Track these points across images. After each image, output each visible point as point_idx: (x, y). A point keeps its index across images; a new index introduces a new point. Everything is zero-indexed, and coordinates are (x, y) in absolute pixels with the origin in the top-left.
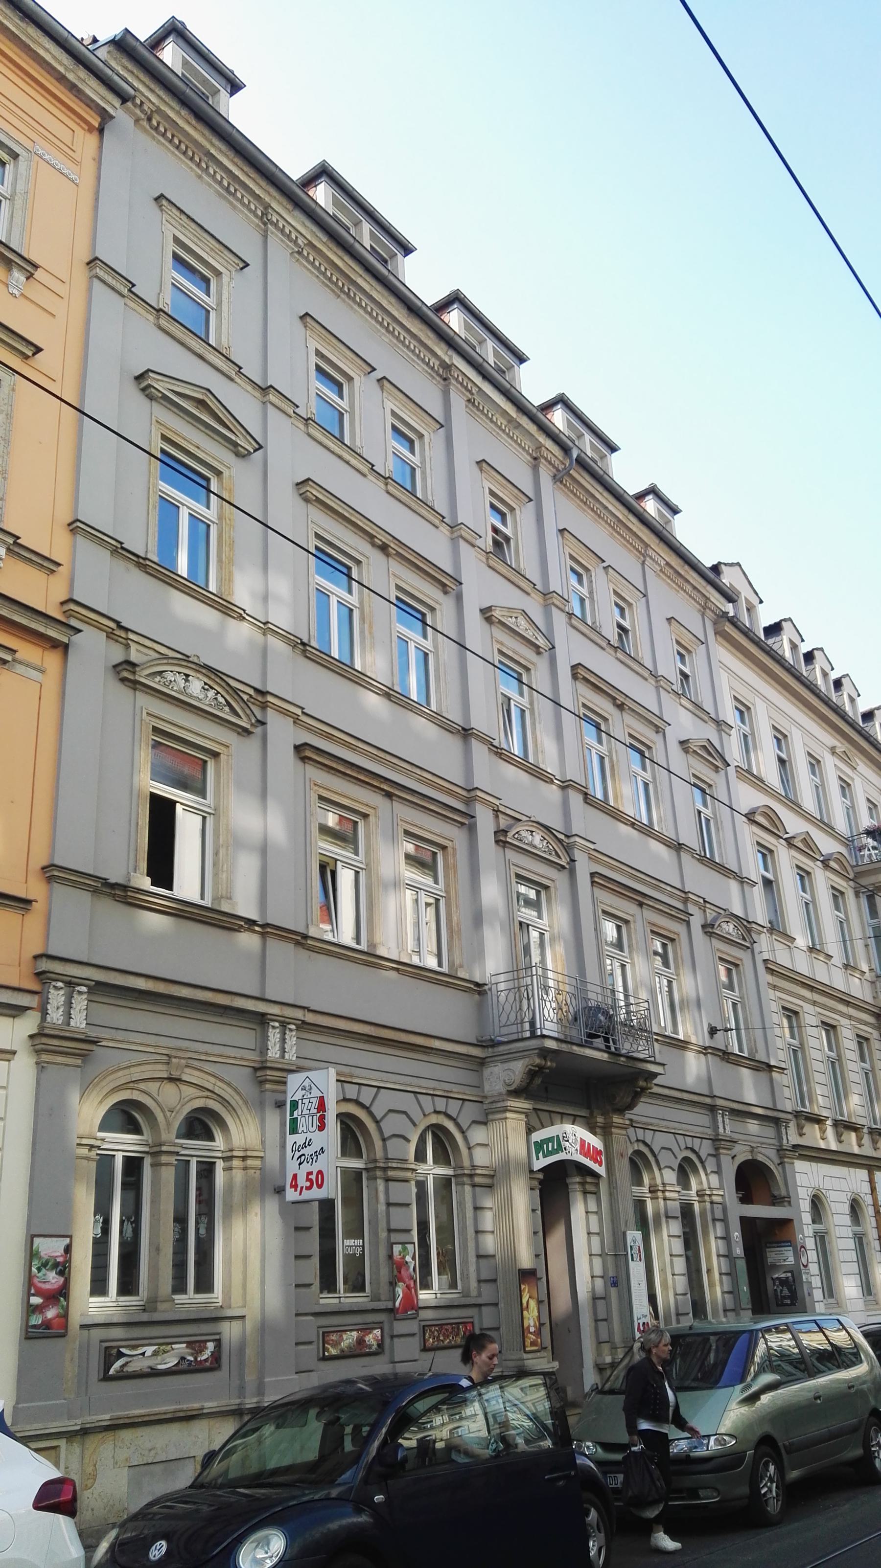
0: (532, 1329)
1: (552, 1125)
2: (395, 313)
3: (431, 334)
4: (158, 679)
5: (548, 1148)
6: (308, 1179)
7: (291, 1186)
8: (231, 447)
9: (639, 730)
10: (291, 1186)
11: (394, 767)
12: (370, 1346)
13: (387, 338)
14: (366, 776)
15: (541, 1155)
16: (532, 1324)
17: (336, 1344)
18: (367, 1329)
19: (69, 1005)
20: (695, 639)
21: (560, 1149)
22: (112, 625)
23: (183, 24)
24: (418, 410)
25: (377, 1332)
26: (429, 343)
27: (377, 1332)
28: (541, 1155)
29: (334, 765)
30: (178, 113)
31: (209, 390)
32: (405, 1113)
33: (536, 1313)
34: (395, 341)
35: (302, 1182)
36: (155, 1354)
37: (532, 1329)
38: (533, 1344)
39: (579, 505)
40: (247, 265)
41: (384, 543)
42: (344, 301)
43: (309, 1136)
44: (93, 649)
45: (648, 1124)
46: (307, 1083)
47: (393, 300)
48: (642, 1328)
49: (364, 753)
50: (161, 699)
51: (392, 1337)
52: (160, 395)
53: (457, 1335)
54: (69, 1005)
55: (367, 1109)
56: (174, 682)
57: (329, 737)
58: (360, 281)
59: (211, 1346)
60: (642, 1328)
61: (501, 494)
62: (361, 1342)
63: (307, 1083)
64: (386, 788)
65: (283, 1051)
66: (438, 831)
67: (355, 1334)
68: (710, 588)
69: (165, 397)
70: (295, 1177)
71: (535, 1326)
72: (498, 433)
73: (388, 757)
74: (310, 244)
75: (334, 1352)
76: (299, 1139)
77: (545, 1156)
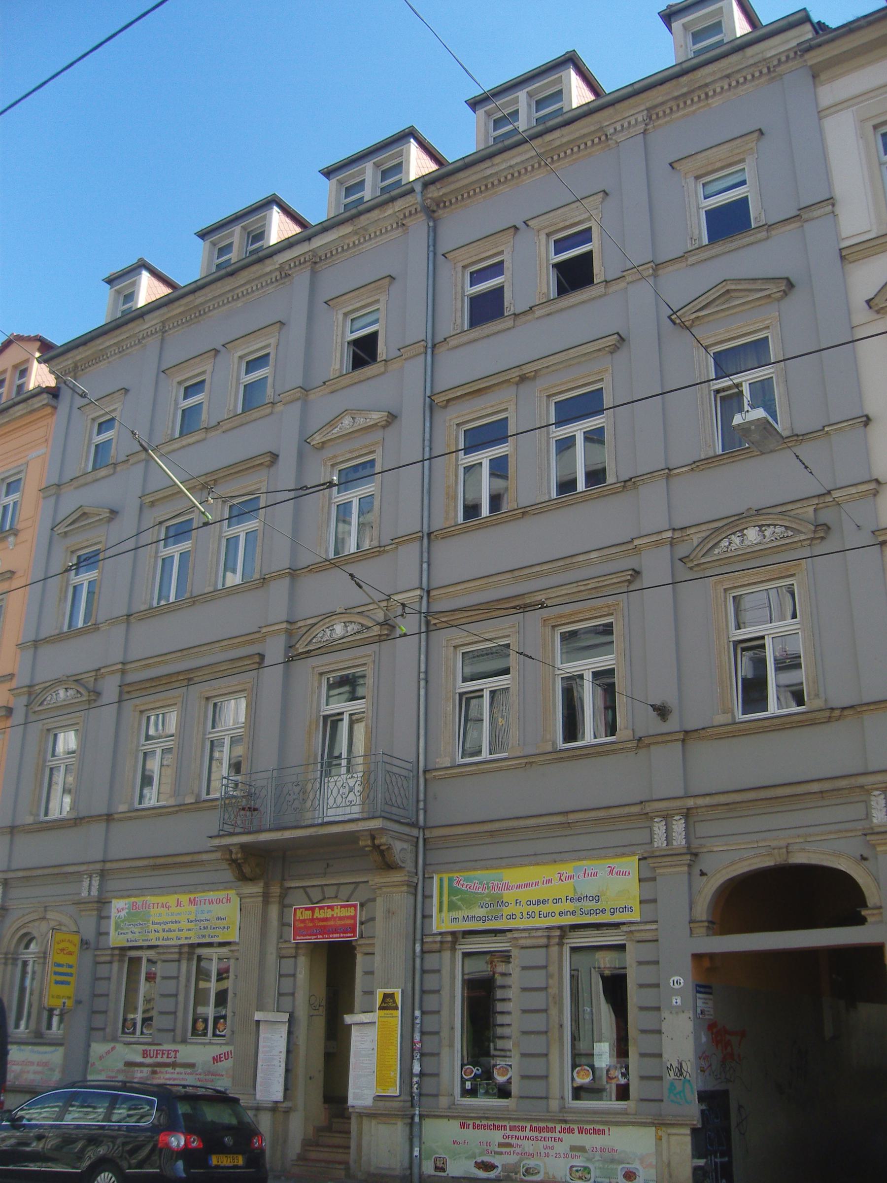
23: (669, 7)
29: (143, 686)
40: (671, 164)
41: (519, 376)
57: (147, 666)
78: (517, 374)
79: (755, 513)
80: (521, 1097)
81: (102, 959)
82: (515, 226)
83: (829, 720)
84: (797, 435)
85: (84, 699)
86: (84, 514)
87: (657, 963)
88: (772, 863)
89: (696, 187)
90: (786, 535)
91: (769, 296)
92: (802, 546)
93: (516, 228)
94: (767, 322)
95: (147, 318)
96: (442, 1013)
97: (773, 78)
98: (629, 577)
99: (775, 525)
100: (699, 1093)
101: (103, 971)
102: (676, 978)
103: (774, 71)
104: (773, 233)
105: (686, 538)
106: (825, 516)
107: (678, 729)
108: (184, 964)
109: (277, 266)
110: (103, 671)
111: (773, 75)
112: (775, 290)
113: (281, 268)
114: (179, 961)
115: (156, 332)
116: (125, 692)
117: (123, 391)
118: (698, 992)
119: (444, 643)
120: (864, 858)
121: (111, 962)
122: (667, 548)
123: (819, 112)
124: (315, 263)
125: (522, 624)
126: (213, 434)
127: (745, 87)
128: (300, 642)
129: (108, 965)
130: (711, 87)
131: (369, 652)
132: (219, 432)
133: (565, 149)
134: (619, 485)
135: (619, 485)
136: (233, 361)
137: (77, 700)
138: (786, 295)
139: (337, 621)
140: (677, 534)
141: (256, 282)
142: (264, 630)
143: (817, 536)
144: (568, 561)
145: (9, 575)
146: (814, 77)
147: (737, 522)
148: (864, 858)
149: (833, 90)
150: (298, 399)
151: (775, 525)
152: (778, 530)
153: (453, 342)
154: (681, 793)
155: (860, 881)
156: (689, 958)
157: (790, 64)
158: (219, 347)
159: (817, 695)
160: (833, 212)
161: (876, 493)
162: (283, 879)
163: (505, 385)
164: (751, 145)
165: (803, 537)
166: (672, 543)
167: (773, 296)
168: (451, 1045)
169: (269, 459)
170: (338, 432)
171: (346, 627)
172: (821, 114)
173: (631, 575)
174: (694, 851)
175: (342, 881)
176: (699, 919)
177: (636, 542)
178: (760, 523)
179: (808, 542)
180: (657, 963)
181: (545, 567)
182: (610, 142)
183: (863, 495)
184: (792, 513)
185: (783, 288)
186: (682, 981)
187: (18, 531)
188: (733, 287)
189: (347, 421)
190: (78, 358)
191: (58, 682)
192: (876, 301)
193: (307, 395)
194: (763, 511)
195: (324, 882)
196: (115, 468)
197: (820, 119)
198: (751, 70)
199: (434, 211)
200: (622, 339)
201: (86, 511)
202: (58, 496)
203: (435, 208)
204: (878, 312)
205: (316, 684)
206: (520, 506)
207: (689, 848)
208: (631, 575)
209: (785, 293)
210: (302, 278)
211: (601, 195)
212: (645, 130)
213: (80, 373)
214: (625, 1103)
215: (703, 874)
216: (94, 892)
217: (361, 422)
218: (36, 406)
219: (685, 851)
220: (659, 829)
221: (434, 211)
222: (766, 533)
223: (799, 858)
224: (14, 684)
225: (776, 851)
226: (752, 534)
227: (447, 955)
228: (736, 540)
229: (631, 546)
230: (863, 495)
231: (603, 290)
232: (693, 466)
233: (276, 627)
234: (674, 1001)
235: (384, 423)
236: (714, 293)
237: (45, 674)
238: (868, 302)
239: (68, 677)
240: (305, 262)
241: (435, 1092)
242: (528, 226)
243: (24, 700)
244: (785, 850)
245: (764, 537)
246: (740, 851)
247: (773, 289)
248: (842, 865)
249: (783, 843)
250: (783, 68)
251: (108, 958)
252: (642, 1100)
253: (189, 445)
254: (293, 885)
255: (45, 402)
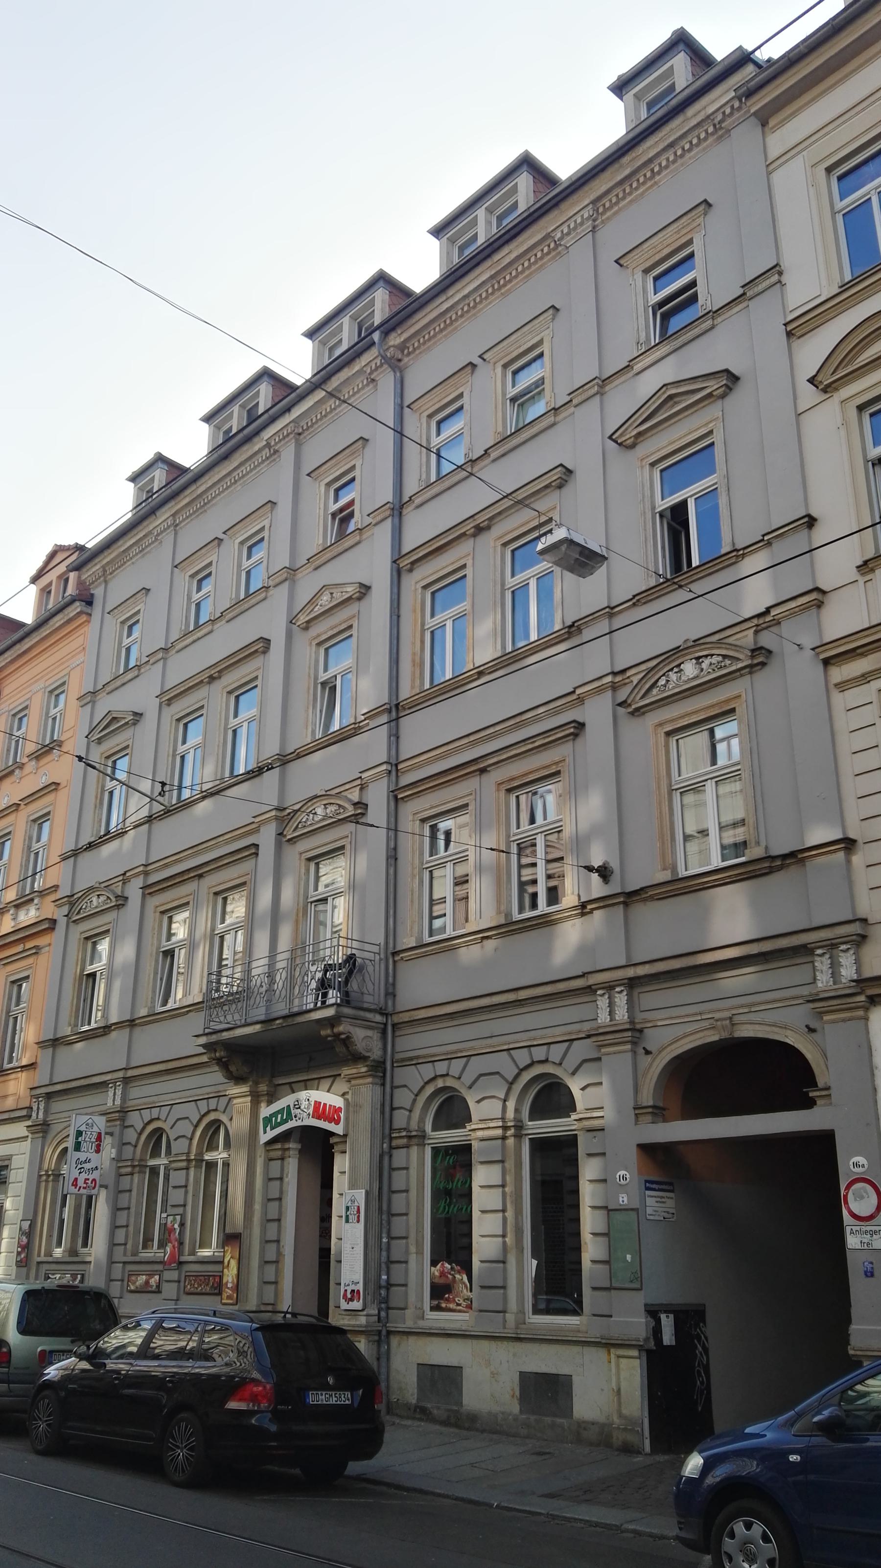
0: (230, 1285)
1: (317, 1089)
2: (224, 473)
3: (245, 448)
4: (655, 691)
5: (276, 1119)
6: (85, 1183)
7: (73, 1185)
8: (548, 490)
9: (516, 525)
10: (73, 1185)
11: (217, 846)
12: (152, 1286)
13: (238, 486)
14: (409, 790)
15: (268, 1128)
16: (230, 1280)
17: (134, 1283)
18: (151, 1276)
19: (611, 1005)
20: (675, 225)
21: (290, 1117)
22: (66, 899)
23: (619, 77)
24: (252, 517)
25: (157, 1277)
26: (250, 453)
27: (157, 1277)
28: (268, 1128)
29: (161, 887)
30: (105, 557)
31: (664, 385)
32: (498, 1073)
33: (235, 1271)
34: (241, 481)
35: (81, 1183)
36: (60, 1278)
37: (230, 1285)
38: (229, 1297)
39: (445, 336)
40: (616, 261)
41: (474, 527)
42: (209, 508)
43: (89, 1156)
44: (598, 714)
45: (456, 1052)
46: (90, 1121)
47: (216, 469)
48: (349, 1296)
49: (429, 762)
50: (663, 706)
51: (179, 1282)
52: (632, 439)
53: (207, 1285)
54: (611, 1005)
55: (203, 1117)
56: (674, 682)
57: (166, 866)
58: (199, 491)
59: (79, 1276)
60: (349, 1296)
61: (338, 473)
62: (147, 1282)
63: (90, 1121)
64: (192, 875)
65: (611, 1013)
66: (236, 875)
67: (144, 1277)
68: (691, 111)
69: (640, 434)
70: (76, 1179)
71: (232, 1282)
72: (337, 414)
73: (200, 847)
74: (174, 515)
75: (132, 1287)
76: (82, 1156)
77: (272, 1129)
78: (472, 525)
79: (692, 644)
80: (481, 1311)
81: (123, 1171)
82: (471, 363)
83: (771, 871)
84: (738, 550)
85: (113, 904)
86: (114, 719)
87: (604, 1154)
88: (716, 1038)
89: (644, 282)
90: (723, 664)
91: (710, 395)
92: (742, 675)
93: (472, 365)
94: (711, 425)
95: (158, 513)
96: (410, 1285)
97: (721, 137)
98: (572, 730)
99: (712, 655)
100: (646, 1305)
101: (125, 1182)
102: (622, 1173)
103: (721, 128)
104: (719, 320)
105: (627, 681)
106: (767, 640)
107: (619, 891)
108: (192, 1172)
109: (265, 443)
110: (128, 874)
111: (720, 133)
112: (716, 387)
113: (268, 445)
114: (187, 1169)
115: (169, 527)
116: (148, 891)
117: (144, 591)
118: (648, 1189)
119: (411, 818)
120: (811, 1030)
121: (132, 1174)
122: (609, 693)
123: (768, 166)
124: (299, 434)
125: (478, 792)
126: (218, 625)
127: (692, 153)
128: (287, 829)
129: (129, 1177)
130: (657, 162)
131: (346, 834)
132: (224, 622)
133: (515, 266)
134: (563, 631)
135: (563, 631)
136: (231, 546)
137: (108, 906)
138: (731, 389)
139: (318, 804)
140: (618, 679)
141: (249, 463)
142: (766, 538)
143: (755, 661)
144: (518, 719)
145: (53, 787)
146: (764, 124)
147: (673, 656)
148: (811, 1030)
149: (782, 138)
150: (286, 580)
151: (712, 655)
152: (715, 660)
153: (418, 501)
154: (623, 962)
155: (808, 1056)
156: (635, 1147)
157: (737, 115)
158: (222, 536)
159: (758, 843)
160: (780, 282)
161: (820, 605)
162: (273, 1076)
163: (463, 539)
164: (698, 221)
165: (740, 665)
166: (614, 687)
167: (714, 393)
168: (420, 1252)
169: (261, 645)
170: (319, 609)
171: (326, 808)
172: (770, 167)
173: (574, 727)
174: (638, 1026)
175: (322, 1075)
176: (645, 1104)
177: (578, 691)
178: (697, 655)
179: (747, 670)
180: (604, 1154)
181: (498, 728)
182: (560, 248)
183: (805, 608)
184: (730, 640)
185: (724, 382)
186: (628, 1176)
187: (62, 742)
188: (674, 391)
189: (326, 598)
190: (105, 562)
191: (91, 889)
192: (819, 378)
193: (294, 575)
194: (701, 641)
195: (306, 1078)
196: (139, 670)
197: (769, 174)
198: (696, 133)
199: (400, 360)
200: (569, 472)
201: (114, 716)
202: (93, 702)
203: (400, 357)
204: (825, 391)
205: (303, 870)
206: (476, 665)
207: (632, 1022)
208: (574, 727)
209: (729, 389)
210: (288, 453)
211: (551, 311)
212: (594, 227)
213: (109, 577)
214: (578, 1318)
215: (648, 1052)
216: (118, 1102)
217: (339, 597)
218: (72, 615)
219: (627, 1026)
220: (603, 1002)
221: (400, 360)
222: (704, 666)
223: (746, 1031)
224: (59, 895)
225: (719, 1023)
226: (690, 669)
227: (414, 1150)
228: (673, 676)
229: (574, 697)
230: (805, 608)
231: (552, 419)
232: (634, 601)
233: (267, 816)
234: (621, 1199)
235: (357, 595)
236: (654, 402)
237: (82, 885)
238: (811, 381)
239: (100, 883)
240: (288, 435)
241: (402, 1306)
242: (484, 360)
243: (65, 910)
244: (728, 1022)
245: (702, 670)
246: (682, 1025)
247: (713, 385)
248: (791, 1039)
249: (727, 1014)
250: (729, 121)
251: (129, 1170)
252: (594, 1315)
253: (199, 639)
254: (280, 1082)
255: (78, 610)
